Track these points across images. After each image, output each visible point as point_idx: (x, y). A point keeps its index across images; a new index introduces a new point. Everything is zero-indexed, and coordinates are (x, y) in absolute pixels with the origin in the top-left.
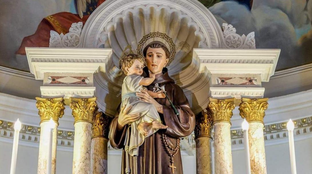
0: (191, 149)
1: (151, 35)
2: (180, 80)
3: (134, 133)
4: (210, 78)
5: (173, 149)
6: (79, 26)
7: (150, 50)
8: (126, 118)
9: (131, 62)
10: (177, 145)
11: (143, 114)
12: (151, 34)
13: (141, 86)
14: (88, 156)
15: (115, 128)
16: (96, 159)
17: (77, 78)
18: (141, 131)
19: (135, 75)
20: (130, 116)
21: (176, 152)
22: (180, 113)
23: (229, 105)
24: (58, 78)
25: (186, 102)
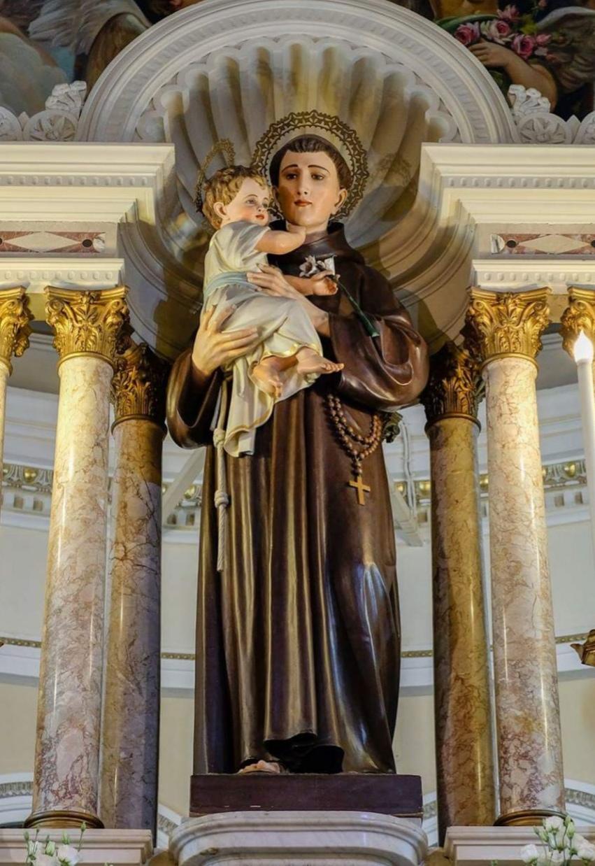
0: (413, 523)
1: (293, 120)
2: (382, 260)
3: (242, 390)
4: (473, 241)
5: (360, 438)
6: (75, 94)
7: (290, 158)
8: (218, 344)
9: (232, 185)
10: (372, 430)
11: (270, 329)
12: (293, 118)
13: (264, 255)
14: (101, 454)
15: (184, 379)
16: (125, 483)
17: (68, 237)
18: (264, 381)
19: (245, 222)
20: (228, 336)
21: (367, 449)
22: (381, 331)
23: (530, 310)
24: (11, 235)
25: (401, 310)
